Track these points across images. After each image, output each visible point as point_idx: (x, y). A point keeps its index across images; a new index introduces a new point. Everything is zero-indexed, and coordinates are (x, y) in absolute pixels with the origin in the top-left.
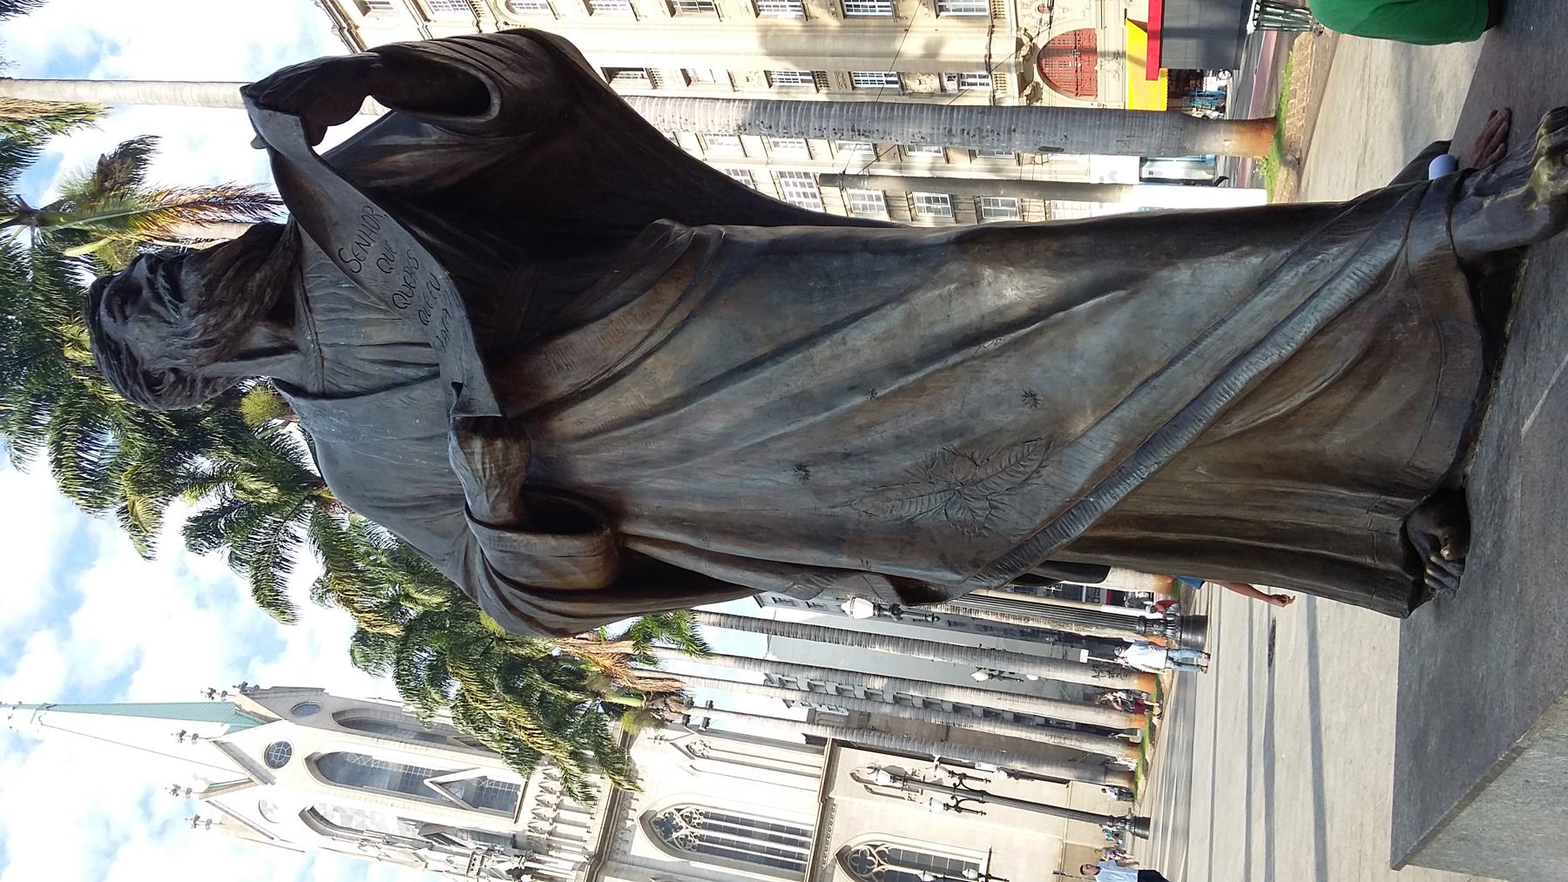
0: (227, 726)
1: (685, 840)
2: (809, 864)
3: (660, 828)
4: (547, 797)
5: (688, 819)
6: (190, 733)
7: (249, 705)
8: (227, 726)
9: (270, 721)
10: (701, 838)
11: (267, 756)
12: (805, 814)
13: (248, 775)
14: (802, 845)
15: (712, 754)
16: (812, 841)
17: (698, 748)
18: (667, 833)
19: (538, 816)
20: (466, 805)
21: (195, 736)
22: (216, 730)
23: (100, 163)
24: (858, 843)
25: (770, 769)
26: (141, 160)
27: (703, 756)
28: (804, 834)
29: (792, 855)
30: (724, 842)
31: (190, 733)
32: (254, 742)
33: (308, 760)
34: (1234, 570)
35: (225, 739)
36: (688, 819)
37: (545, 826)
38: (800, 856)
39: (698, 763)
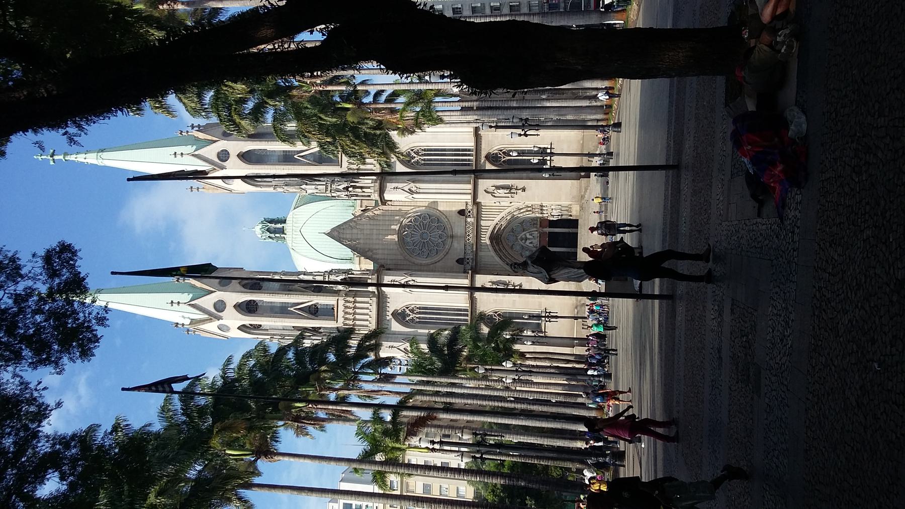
0: (195, 147)
1: (417, 162)
2: (474, 163)
3: (400, 316)
4: (348, 310)
5: (417, 153)
6: (179, 152)
7: (201, 135)
8: (195, 147)
9: (215, 141)
10: (424, 160)
11: (219, 157)
12: (470, 144)
13: (206, 316)
14: (469, 155)
15: (421, 191)
16: (474, 153)
17: (413, 189)
18: (404, 318)
19: (346, 319)
20: (310, 316)
21: (182, 154)
22: (190, 149)
23: (70, 245)
24: (494, 149)
25: (446, 288)
26: (90, 349)
27: (417, 193)
28: (469, 150)
29: (465, 160)
30: (430, 319)
31: (179, 152)
32: (211, 152)
33: (234, 306)
34: (632, 149)
35: (196, 153)
36: (412, 311)
37: (351, 322)
38: (469, 160)
39: (415, 196)
